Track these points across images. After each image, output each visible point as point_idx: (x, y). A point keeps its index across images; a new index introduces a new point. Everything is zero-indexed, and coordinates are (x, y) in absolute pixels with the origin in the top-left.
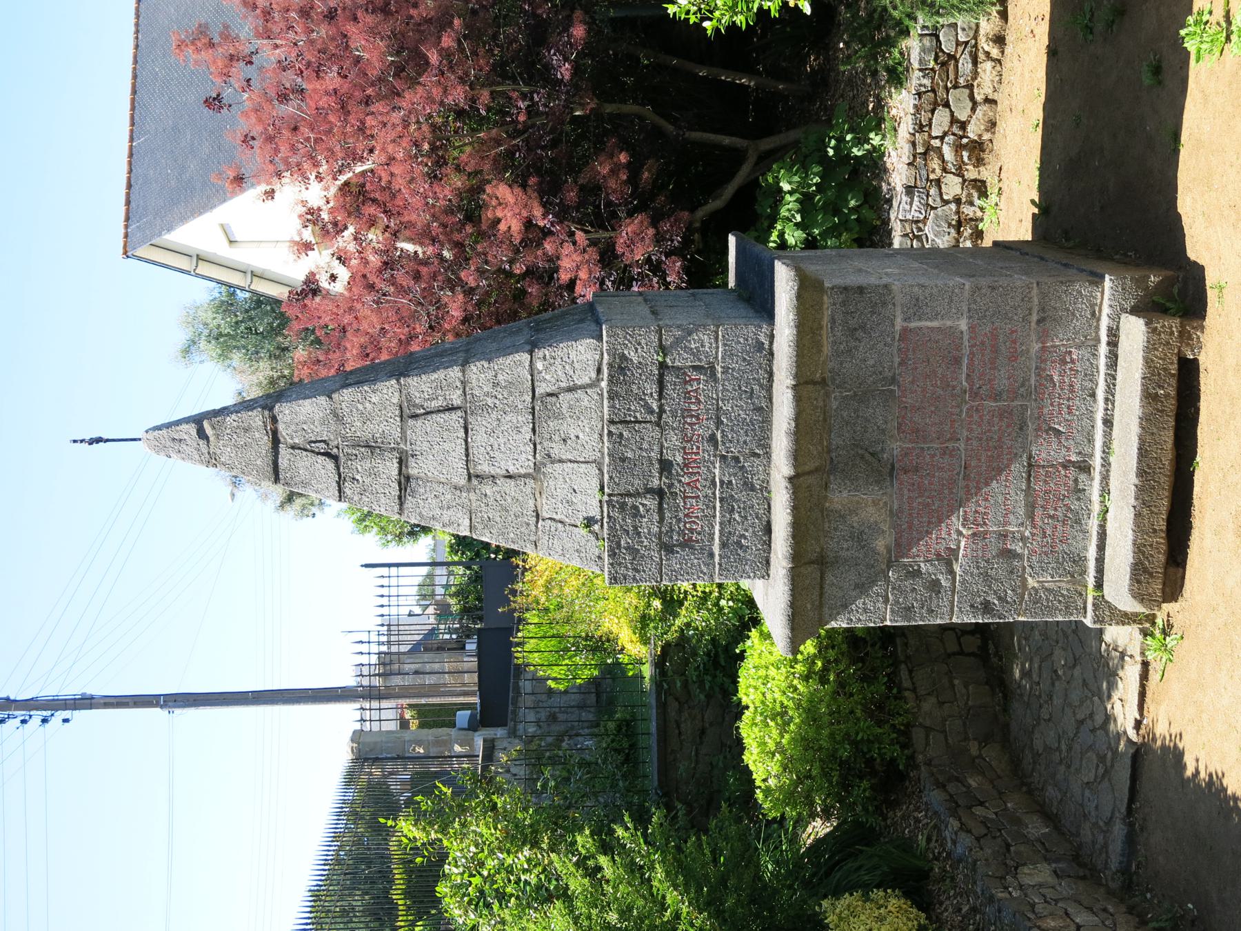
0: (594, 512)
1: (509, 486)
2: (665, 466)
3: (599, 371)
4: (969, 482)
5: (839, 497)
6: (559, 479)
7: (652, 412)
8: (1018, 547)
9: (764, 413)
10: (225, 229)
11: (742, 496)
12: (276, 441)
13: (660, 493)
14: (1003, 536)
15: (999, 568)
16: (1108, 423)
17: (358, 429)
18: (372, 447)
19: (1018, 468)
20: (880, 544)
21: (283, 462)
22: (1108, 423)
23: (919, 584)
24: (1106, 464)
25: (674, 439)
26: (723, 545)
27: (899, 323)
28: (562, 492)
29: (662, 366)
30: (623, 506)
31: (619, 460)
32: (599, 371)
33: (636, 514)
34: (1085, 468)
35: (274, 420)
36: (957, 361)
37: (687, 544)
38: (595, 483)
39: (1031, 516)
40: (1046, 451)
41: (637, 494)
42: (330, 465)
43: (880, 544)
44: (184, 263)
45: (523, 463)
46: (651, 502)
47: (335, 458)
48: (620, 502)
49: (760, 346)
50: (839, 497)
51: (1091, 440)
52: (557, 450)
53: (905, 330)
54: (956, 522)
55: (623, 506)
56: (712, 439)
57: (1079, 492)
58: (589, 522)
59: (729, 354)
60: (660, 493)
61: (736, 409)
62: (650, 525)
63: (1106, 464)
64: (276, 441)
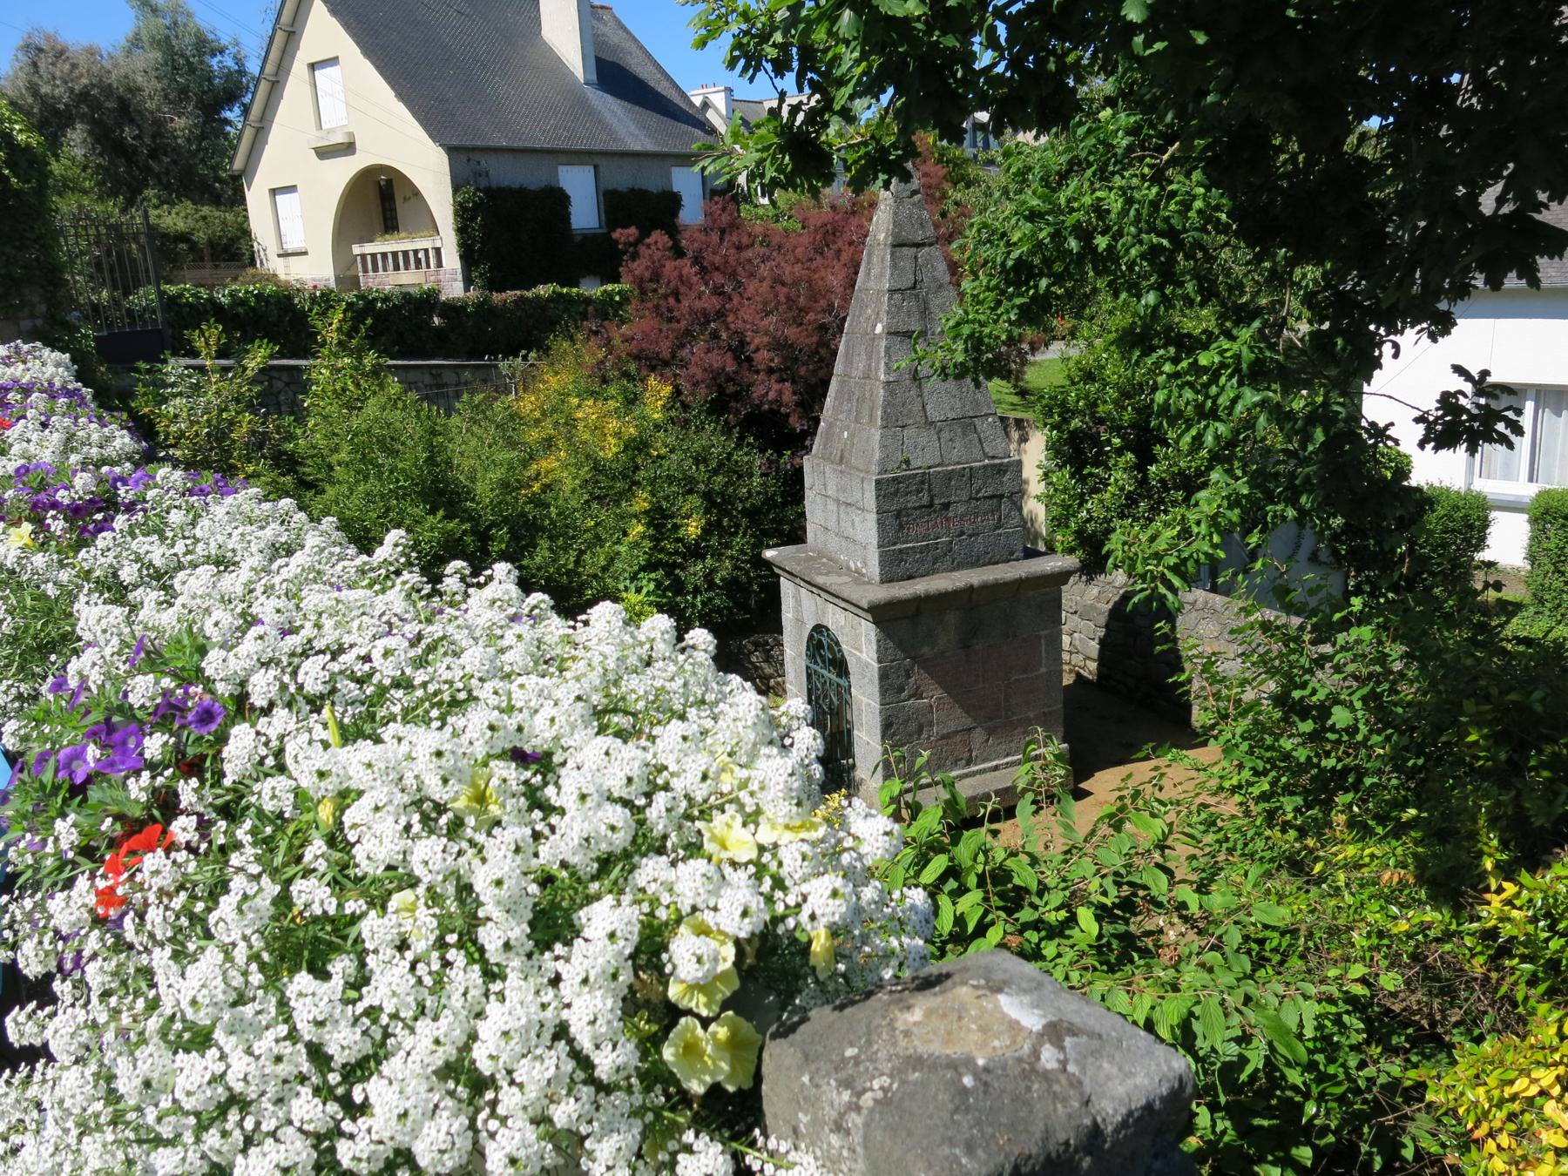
0: (914, 464)
1: (917, 407)
2: (946, 506)
3: (993, 457)
4: (959, 693)
5: (952, 618)
6: (926, 438)
7: (978, 492)
8: (924, 735)
9: (976, 563)
10: (333, 61)
11: (930, 558)
12: (918, 245)
13: (931, 505)
14: (931, 724)
15: (913, 726)
16: (996, 768)
17: (935, 302)
18: (925, 312)
19: (969, 722)
20: (925, 650)
21: (905, 250)
22: (996, 768)
23: (902, 679)
24: (974, 774)
25: (961, 509)
26: (901, 551)
27: (1043, 633)
28: (922, 441)
29: (1002, 496)
30: (923, 482)
31: (949, 476)
32: (993, 457)
33: (919, 491)
34: (968, 763)
35: (931, 245)
36: (1025, 671)
37: (901, 527)
38: (931, 463)
39: (943, 737)
40: (978, 736)
41: (930, 490)
42: (910, 284)
43: (925, 650)
44: (286, 17)
45: (933, 414)
46: (925, 500)
47: (914, 288)
48: (924, 480)
49: (1012, 553)
50: (952, 618)
51: (984, 761)
52: (945, 435)
53: (1039, 637)
54: (938, 693)
55: (923, 482)
56: (963, 533)
57: (955, 764)
58: (907, 462)
59: (1008, 535)
60: (931, 505)
61: (979, 544)
62: (912, 501)
63: (974, 774)
64: (918, 245)
